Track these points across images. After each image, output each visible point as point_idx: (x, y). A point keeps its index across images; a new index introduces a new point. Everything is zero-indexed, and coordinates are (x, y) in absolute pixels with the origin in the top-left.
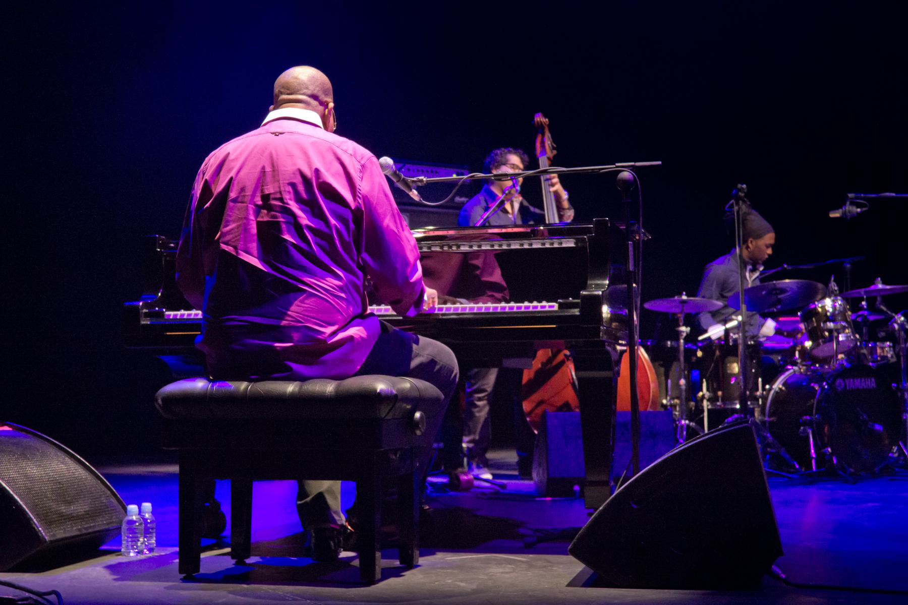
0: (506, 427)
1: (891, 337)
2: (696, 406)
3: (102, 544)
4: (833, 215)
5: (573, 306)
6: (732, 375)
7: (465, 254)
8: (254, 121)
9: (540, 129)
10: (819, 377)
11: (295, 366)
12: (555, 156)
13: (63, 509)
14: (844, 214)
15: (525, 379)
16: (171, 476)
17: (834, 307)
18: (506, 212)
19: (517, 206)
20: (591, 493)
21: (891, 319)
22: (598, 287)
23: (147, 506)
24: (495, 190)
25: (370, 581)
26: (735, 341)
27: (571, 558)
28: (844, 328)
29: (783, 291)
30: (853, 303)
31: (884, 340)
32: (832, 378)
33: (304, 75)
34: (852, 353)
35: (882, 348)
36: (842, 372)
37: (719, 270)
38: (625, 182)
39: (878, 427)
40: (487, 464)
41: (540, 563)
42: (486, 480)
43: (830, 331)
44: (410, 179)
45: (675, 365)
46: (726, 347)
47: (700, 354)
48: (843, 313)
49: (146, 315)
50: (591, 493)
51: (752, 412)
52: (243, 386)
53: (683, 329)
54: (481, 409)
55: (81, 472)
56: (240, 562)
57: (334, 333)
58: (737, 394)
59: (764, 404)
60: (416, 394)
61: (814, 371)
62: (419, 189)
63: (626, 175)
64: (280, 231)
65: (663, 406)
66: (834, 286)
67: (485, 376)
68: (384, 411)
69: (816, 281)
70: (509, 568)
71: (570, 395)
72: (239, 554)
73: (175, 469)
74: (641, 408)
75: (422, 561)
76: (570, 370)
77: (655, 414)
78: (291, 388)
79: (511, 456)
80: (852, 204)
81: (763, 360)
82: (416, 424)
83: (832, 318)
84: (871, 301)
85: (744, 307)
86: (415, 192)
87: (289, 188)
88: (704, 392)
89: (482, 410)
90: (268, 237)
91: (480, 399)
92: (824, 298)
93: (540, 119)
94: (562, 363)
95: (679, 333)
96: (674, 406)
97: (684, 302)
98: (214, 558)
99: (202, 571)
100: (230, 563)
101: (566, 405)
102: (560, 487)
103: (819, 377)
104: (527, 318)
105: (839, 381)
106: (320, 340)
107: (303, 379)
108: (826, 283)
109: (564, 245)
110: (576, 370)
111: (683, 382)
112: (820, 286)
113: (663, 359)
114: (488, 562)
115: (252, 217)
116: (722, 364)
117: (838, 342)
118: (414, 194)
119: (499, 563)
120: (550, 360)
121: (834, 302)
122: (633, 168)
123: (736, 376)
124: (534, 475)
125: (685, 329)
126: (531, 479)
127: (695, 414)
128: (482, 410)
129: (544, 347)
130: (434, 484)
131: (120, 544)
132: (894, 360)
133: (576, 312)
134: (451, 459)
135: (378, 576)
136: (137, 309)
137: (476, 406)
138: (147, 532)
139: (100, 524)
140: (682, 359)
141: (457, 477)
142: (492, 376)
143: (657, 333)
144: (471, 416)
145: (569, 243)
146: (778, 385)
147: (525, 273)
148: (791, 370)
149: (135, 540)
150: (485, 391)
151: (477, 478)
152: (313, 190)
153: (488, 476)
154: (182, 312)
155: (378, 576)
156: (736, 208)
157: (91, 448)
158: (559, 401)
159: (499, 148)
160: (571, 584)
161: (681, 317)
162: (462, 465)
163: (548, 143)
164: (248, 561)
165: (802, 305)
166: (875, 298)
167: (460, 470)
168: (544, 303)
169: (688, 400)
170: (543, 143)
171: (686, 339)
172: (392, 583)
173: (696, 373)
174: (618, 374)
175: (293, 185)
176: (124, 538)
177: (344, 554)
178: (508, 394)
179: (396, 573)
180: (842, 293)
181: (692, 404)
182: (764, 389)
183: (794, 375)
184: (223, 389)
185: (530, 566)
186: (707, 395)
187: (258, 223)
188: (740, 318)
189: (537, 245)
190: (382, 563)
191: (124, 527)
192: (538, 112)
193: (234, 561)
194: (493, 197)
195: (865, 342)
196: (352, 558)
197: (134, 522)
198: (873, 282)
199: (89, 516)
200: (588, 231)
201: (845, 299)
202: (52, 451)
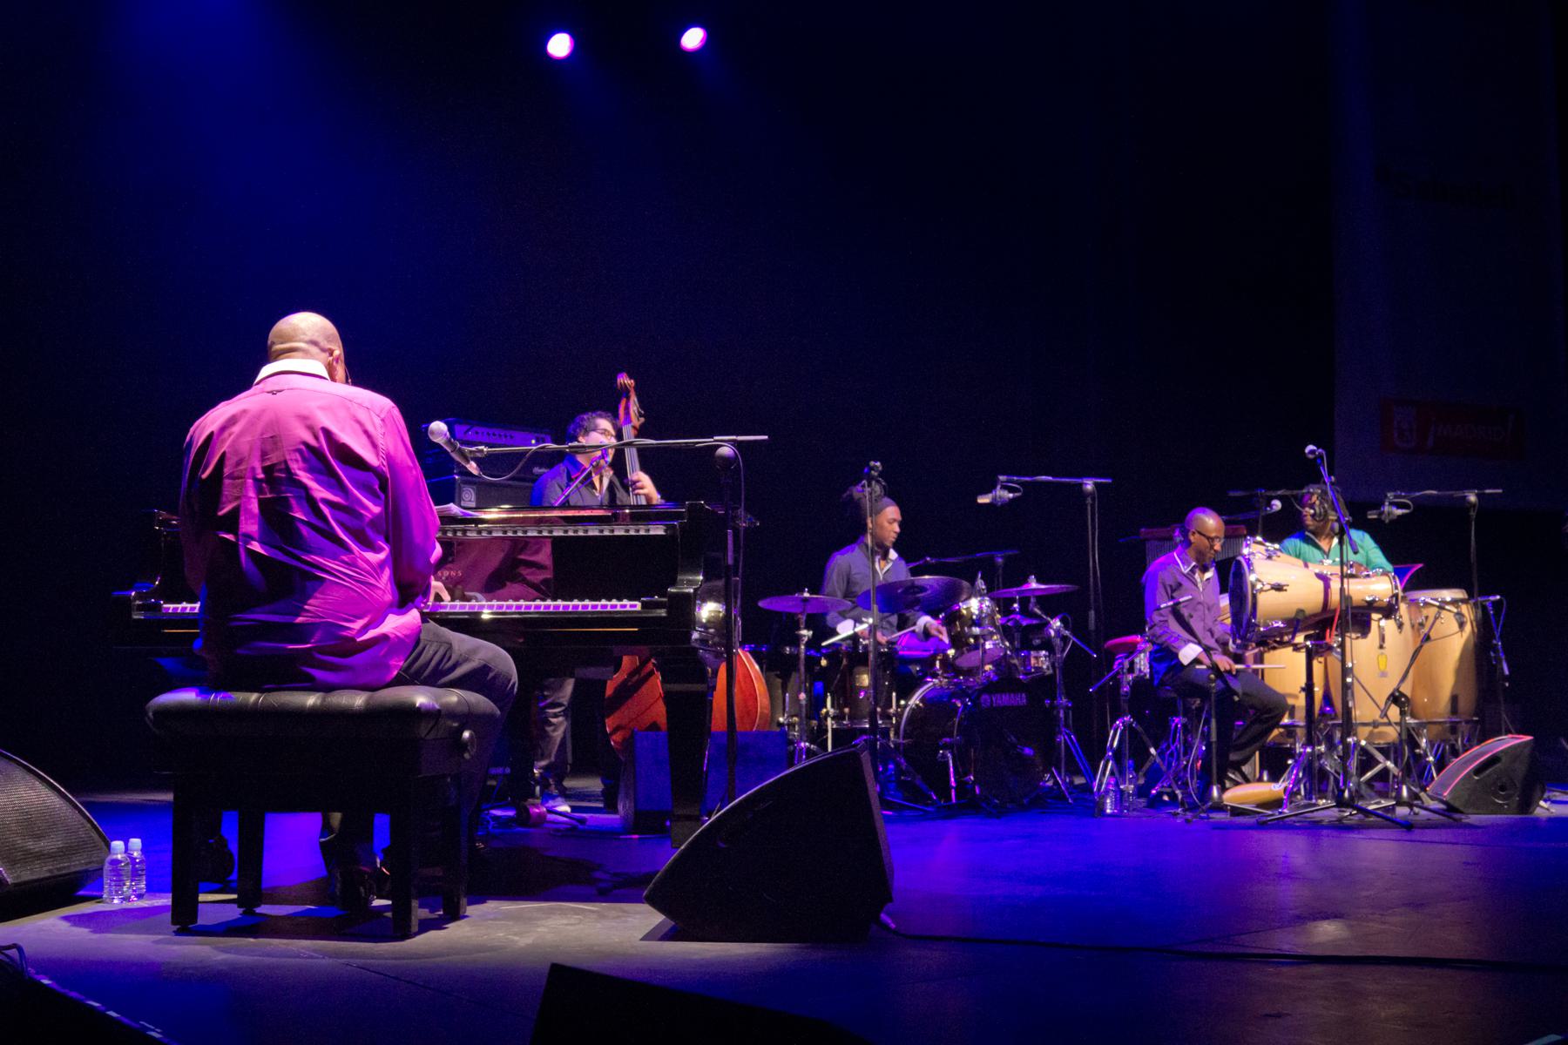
0: (588, 751)
1: (1047, 645)
2: (819, 726)
3: (82, 887)
4: (984, 500)
5: (658, 605)
6: (861, 689)
7: (515, 540)
8: (243, 380)
9: (625, 392)
10: (961, 693)
11: (318, 674)
12: (642, 426)
13: (31, 845)
14: (994, 499)
15: (609, 692)
16: (166, 804)
17: (981, 609)
18: (594, 487)
19: (606, 482)
20: (677, 829)
21: (1048, 624)
22: (690, 583)
23: (136, 843)
24: (581, 459)
25: (404, 934)
26: (866, 647)
27: (646, 907)
28: (992, 634)
29: (923, 589)
30: (1004, 606)
31: (1038, 648)
32: (976, 696)
33: (307, 324)
34: (1001, 663)
35: (1037, 658)
36: (990, 687)
37: (847, 564)
38: (724, 459)
39: (1027, 751)
40: (566, 795)
41: (614, 913)
42: (561, 814)
43: (976, 637)
44: (467, 449)
45: (794, 675)
46: (854, 653)
47: (824, 662)
48: (991, 616)
49: (140, 608)
50: (677, 829)
51: (885, 733)
52: (253, 697)
53: (804, 632)
54: (556, 726)
55: (54, 800)
56: (248, 912)
57: (365, 629)
58: (866, 710)
59: (898, 723)
60: (465, 709)
61: (958, 685)
62: (478, 461)
63: (726, 450)
64: (290, 508)
65: (780, 725)
66: (980, 584)
67: (561, 687)
68: (423, 729)
69: (963, 574)
70: (574, 919)
71: (659, 712)
72: (249, 899)
73: (169, 797)
74: (739, 727)
75: (471, 910)
76: (658, 678)
77: (764, 735)
78: (312, 700)
79: (594, 785)
80: (1004, 488)
81: (899, 671)
82: (463, 746)
83: (978, 623)
84: (1024, 602)
85: (875, 607)
86: (473, 464)
87: (298, 456)
88: (829, 707)
89: (559, 727)
90: (275, 518)
91: (556, 716)
92: (969, 598)
93: (625, 380)
94: (651, 673)
95: (799, 638)
96: (791, 725)
97: (806, 600)
98: (214, 903)
99: (200, 922)
100: (235, 912)
101: (654, 726)
102: (652, 823)
103: (961, 693)
104: (555, 620)
105: (984, 697)
106: (346, 638)
107: (328, 688)
108: (973, 582)
109: (652, 533)
110: (663, 682)
111: (803, 696)
112: (965, 584)
113: (777, 666)
114: (551, 911)
115: (251, 494)
116: (850, 674)
117: (985, 651)
118: (472, 467)
119: (563, 913)
120: (637, 671)
121: (981, 603)
122: (734, 442)
123: (865, 689)
124: (620, 807)
125: (806, 633)
126: (616, 812)
127: (818, 736)
128: (559, 727)
129: (632, 654)
130: (496, 818)
131: (101, 889)
132: (1050, 672)
133: (663, 613)
134: (518, 789)
135: (415, 929)
136: (129, 601)
137: (551, 724)
138: (135, 875)
139: (77, 864)
140: (802, 669)
141: (527, 811)
142: (569, 686)
143: (768, 636)
144: (545, 736)
145: (658, 530)
146: (915, 700)
147: (581, 565)
148: (932, 683)
149: (120, 883)
150: (560, 705)
151: (551, 811)
152: (329, 456)
153: (565, 808)
154: (184, 604)
155: (415, 929)
156: (868, 489)
157: (67, 771)
158: (647, 719)
159: (585, 412)
160: (646, 938)
161: (803, 618)
162: (533, 796)
163: (634, 408)
164: (258, 910)
165: (943, 605)
166: (1028, 599)
167: (531, 801)
168: (625, 602)
169: (809, 717)
170: (627, 408)
171: (807, 644)
172: (433, 936)
173: (819, 685)
174: (714, 688)
175: (299, 451)
176: (106, 881)
177: (377, 902)
178: (589, 708)
179: (438, 924)
180: (990, 592)
181: (815, 722)
182: (898, 706)
183: (934, 689)
184: (229, 701)
185: (601, 916)
186: (832, 711)
187: (261, 502)
188: (871, 621)
189: (619, 532)
190: (420, 913)
191: (107, 867)
192: (621, 371)
193: (241, 910)
194: (579, 467)
195: (1016, 651)
196: (385, 908)
197: (119, 862)
198: (1025, 581)
199: (66, 852)
200: (678, 516)
201: (992, 599)
202: (19, 773)
